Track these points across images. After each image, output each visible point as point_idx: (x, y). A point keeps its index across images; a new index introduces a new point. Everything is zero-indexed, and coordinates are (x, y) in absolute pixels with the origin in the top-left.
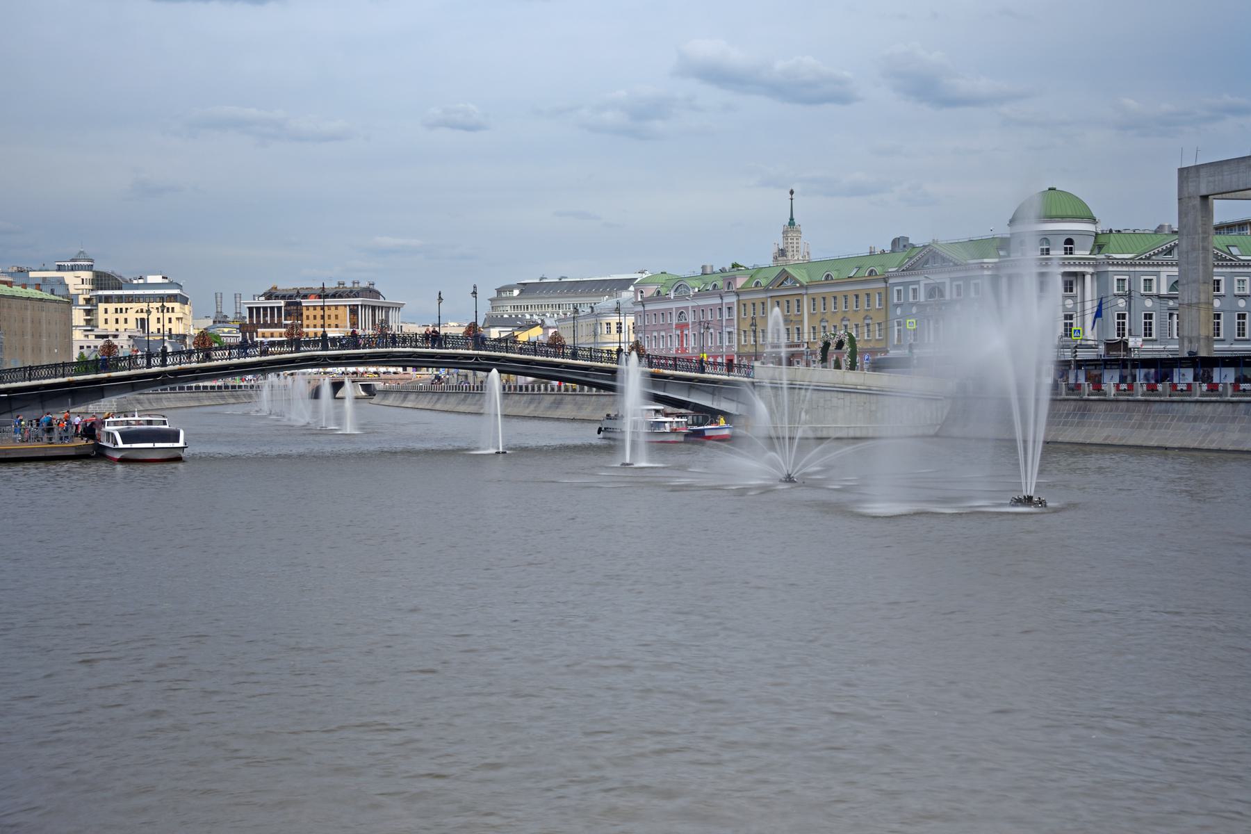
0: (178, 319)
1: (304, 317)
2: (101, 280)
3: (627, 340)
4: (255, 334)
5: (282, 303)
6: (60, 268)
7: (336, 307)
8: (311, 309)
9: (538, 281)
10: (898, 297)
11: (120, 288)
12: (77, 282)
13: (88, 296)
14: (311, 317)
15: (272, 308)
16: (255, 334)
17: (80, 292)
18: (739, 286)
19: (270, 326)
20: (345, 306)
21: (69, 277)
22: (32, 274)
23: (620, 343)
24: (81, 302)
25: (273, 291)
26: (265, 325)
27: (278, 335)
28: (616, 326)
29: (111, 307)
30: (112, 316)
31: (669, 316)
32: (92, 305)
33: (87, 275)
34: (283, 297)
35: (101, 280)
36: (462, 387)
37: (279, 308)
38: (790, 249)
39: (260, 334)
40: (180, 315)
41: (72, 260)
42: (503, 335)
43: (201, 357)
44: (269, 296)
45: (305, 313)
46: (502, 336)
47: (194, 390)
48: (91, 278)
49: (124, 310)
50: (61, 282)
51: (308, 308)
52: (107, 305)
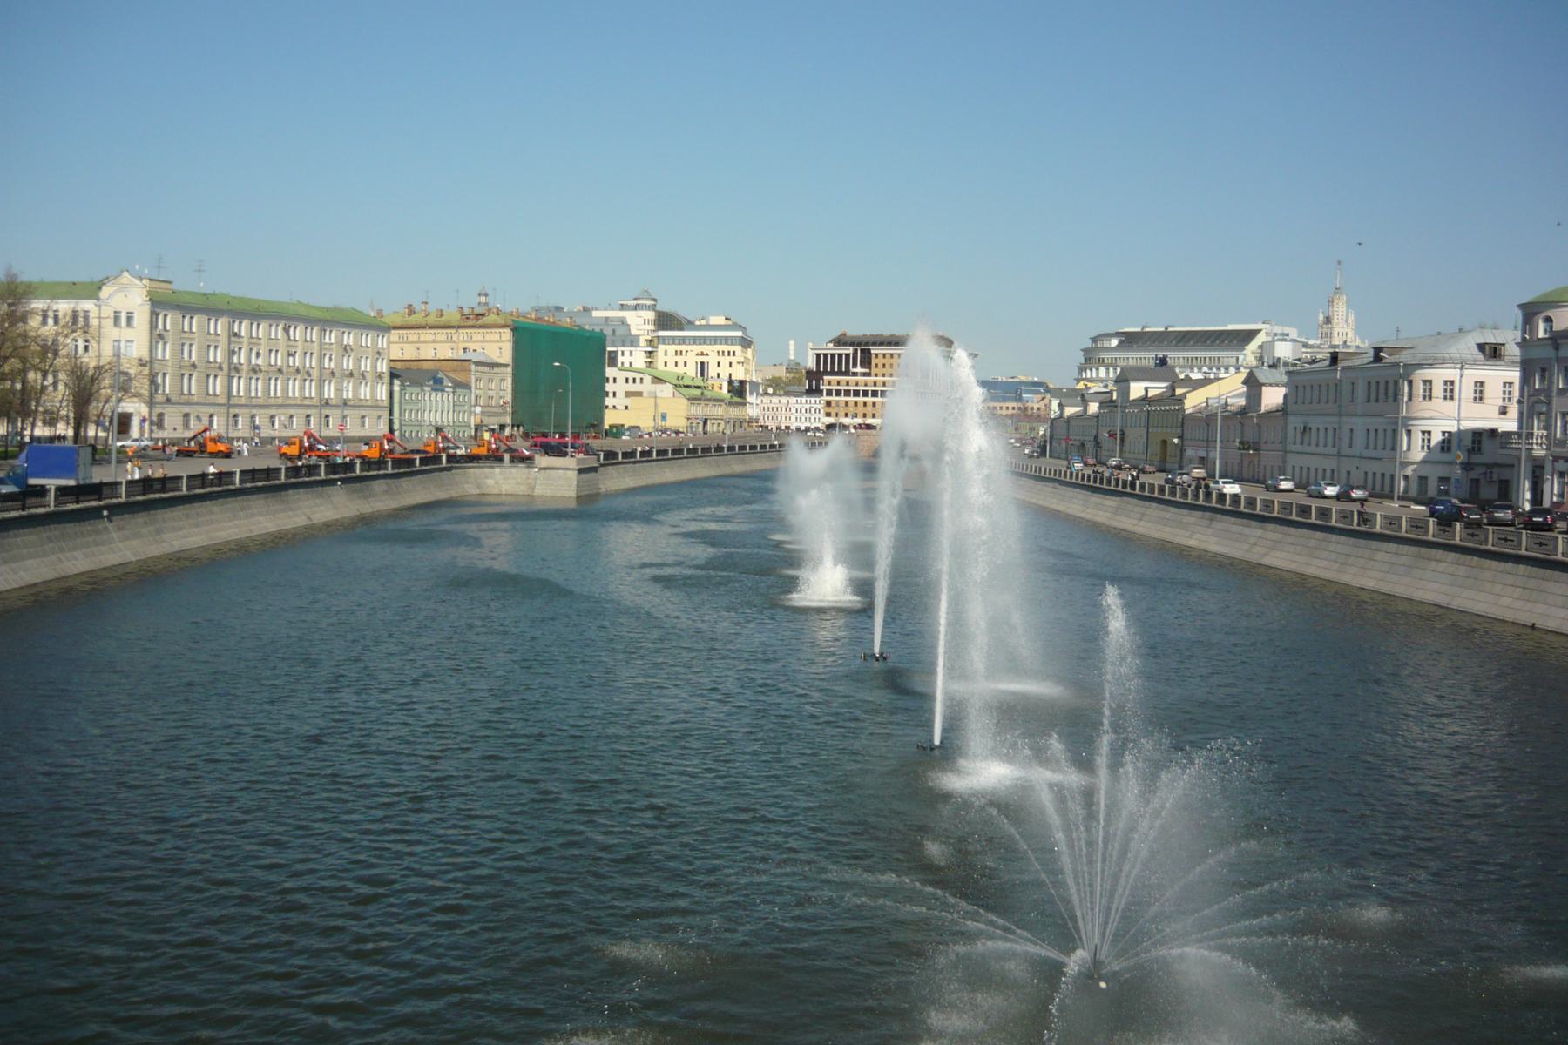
0: (739, 363)
2: (665, 321)
4: (868, 371)
5: (850, 350)
6: (623, 307)
9: (1139, 330)
11: (682, 329)
12: (640, 323)
13: (649, 338)
14: (880, 365)
15: (840, 355)
16: (868, 371)
17: (642, 332)
19: (840, 373)
22: (595, 314)
23: (1459, 420)
24: (642, 342)
26: (833, 373)
28: (1472, 388)
29: (671, 349)
30: (671, 359)
32: (653, 347)
33: (651, 315)
34: (852, 344)
35: (665, 321)
37: (847, 355)
38: (1336, 317)
39: (826, 382)
40: (742, 360)
41: (635, 299)
42: (1151, 393)
43: (1542, 326)
44: (839, 342)
46: (1149, 395)
47: (670, 456)
48: (653, 318)
49: (684, 353)
50: (623, 322)
51: (877, 355)
52: (667, 347)
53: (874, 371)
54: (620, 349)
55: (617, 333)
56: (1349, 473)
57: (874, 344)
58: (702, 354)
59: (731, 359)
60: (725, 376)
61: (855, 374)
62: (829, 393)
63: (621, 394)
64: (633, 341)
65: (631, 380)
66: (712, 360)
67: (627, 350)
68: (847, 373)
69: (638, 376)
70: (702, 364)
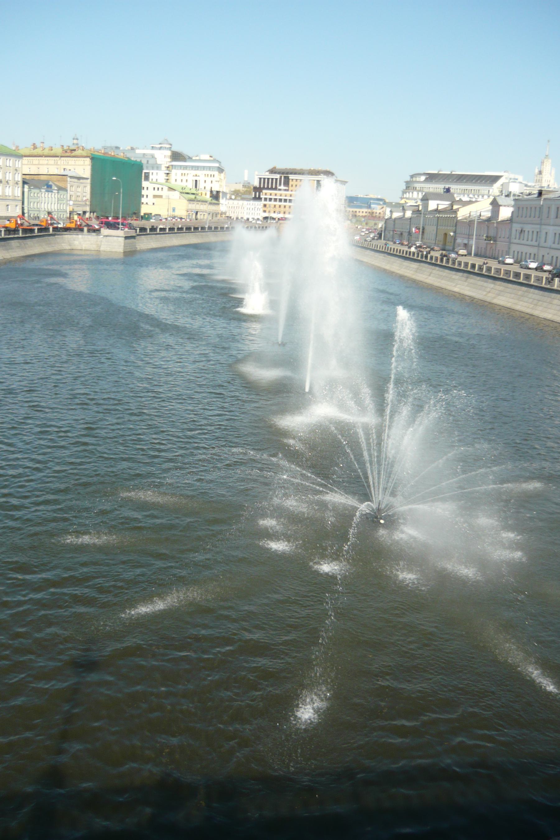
1: (290, 185)
2: (176, 156)
3: (468, 233)
4: (286, 188)
5: (278, 176)
7: (297, 180)
8: (294, 181)
10: (300, 174)
15: (272, 179)
16: (286, 188)
18: (365, 210)
19: (272, 189)
20: (314, 180)
21: (157, 153)
22: (138, 151)
25: (274, 169)
26: (268, 188)
27: (284, 195)
29: (179, 172)
30: (179, 178)
31: (239, 472)
32: (169, 171)
33: (169, 153)
34: (279, 173)
35: (176, 156)
36: (373, 244)
37: (276, 179)
44: (272, 171)
45: (291, 183)
51: (292, 179)
53: (290, 188)
54: (151, 172)
55: (150, 162)
56: (543, 256)
57: (291, 173)
58: (196, 176)
59: (212, 179)
60: (208, 189)
61: (280, 190)
62: (266, 199)
63: (151, 196)
64: (158, 167)
65: (156, 189)
66: (201, 180)
67: (155, 172)
68: (276, 189)
69: (160, 187)
70: (196, 181)
